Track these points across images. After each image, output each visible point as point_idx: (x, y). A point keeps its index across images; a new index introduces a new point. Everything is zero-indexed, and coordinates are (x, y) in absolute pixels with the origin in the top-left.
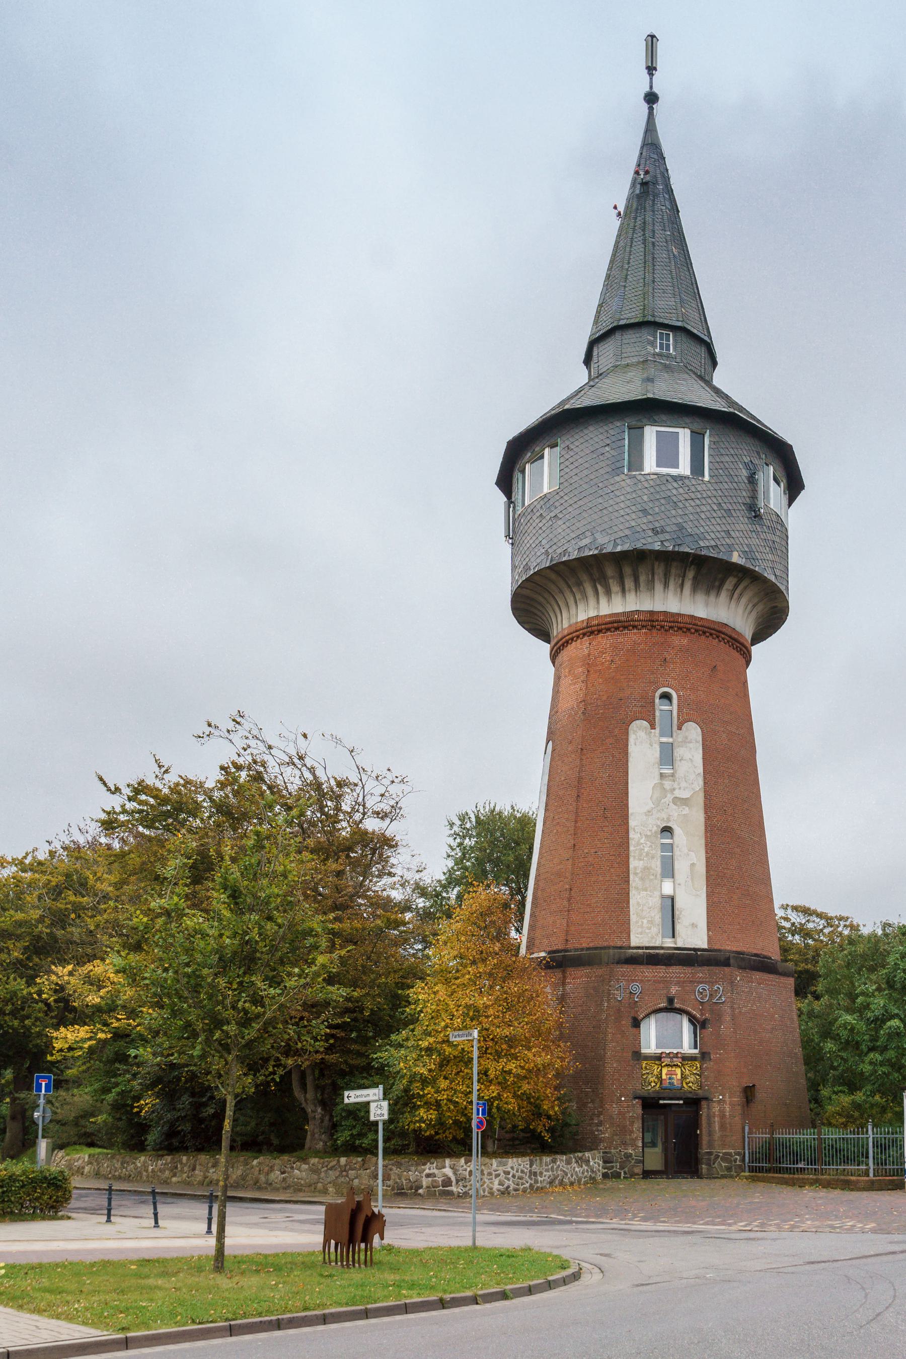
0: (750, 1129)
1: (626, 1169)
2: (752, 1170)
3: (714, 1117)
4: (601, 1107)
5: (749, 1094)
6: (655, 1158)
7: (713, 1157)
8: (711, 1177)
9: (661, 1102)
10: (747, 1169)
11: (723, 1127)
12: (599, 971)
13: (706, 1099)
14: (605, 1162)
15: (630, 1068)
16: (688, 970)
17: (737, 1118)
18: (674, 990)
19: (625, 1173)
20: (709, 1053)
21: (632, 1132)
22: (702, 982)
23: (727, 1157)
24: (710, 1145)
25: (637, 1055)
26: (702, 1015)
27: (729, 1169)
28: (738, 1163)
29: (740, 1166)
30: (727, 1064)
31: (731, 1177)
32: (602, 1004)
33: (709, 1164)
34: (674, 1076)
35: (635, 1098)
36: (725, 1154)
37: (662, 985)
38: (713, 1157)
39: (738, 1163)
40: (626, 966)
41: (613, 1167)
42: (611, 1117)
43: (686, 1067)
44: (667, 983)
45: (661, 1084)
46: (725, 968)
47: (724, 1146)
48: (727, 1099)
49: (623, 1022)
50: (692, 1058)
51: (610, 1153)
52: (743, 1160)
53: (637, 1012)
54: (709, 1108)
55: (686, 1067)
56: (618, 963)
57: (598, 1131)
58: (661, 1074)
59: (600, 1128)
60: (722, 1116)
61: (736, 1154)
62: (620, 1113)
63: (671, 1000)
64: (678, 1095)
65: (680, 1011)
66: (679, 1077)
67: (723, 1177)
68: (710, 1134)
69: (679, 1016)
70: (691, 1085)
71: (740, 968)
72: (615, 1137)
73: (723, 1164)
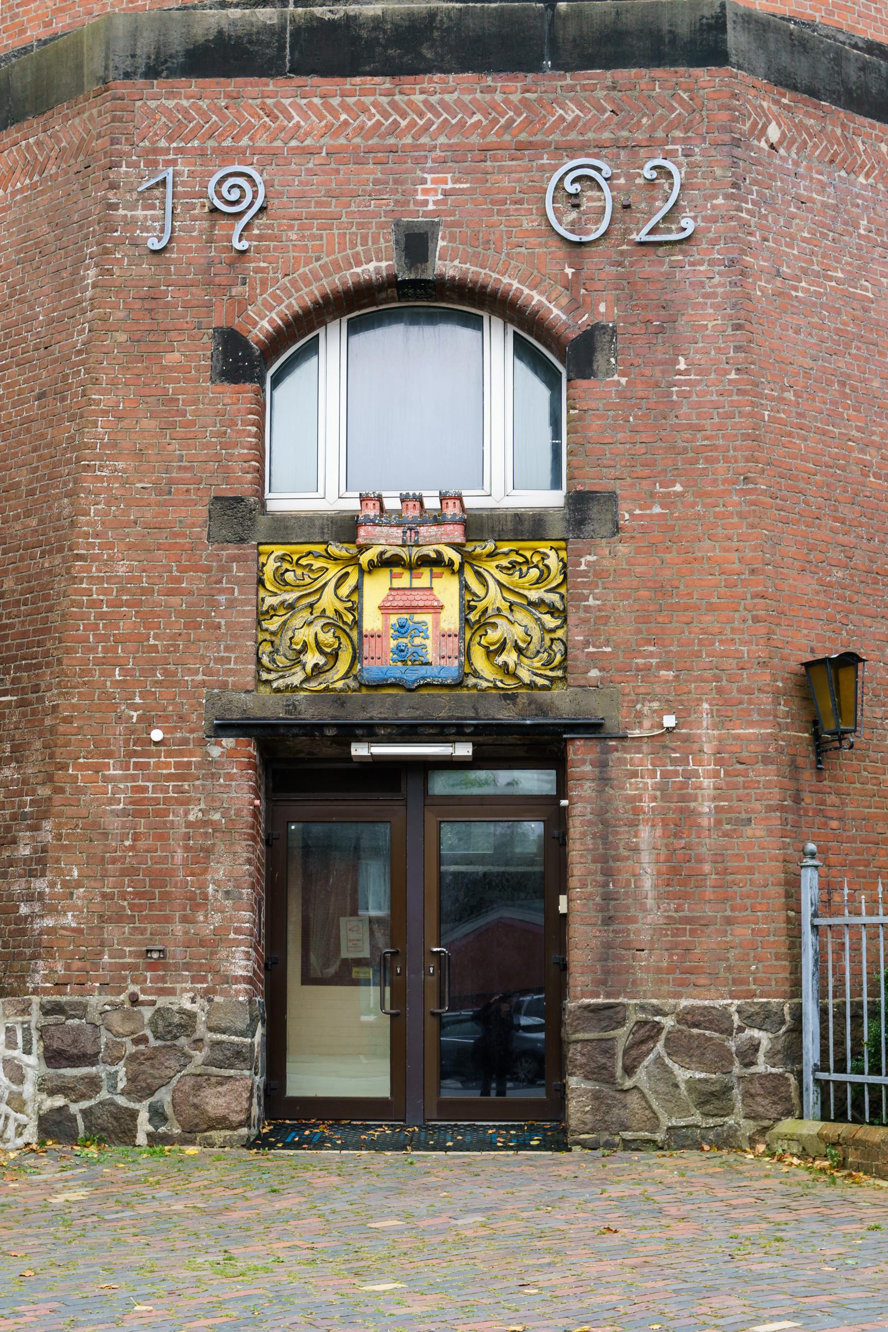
0: (828, 887)
1: (164, 1096)
2: (838, 1106)
3: (633, 824)
4: (50, 779)
5: (826, 704)
6: (346, 1048)
7: (622, 1036)
8: (615, 1138)
9: (359, 750)
10: (812, 1096)
11: (678, 874)
12: (69, 127)
13: (592, 729)
14: (53, 1057)
15: (194, 582)
16: (507, 91)
17: (756, 831)
18: (431, 193)
19: (157, 1115)
20: (612, 497)
21: (197, 902)
22: (572, 150)
23: (699, 1036)
24: (612, 968)
25: (239, 515)
26: (575, 307)
27: (713, 1099)
28: (762, 1067)
29: (774, 1087)
30: (707, 548)
31: (726, 1141)
32: (75, 281)
33: (600, 1073)
34: (417, 625)
35: (223, 729)
36: (689, 1018)
37: (372, 172)
38: (622, 1036)
39: (762, 1067)
40: (194, 85)
41: (94, 1084)
42: (95, 828)
43: (490, 567)
44: (395, 158)
45: (356, 657)
46: (702, 74)
47: (685, 975)
48: (706, 733)
49: (174, 358)
50: (528, 526)
51: (80, 1010)
52: (792, 1052)
53: (242, 305)
54: (604, 780)
55: (490, 567)
56: (152, 73)
57: (29, 898)
58: (356, 609)
59: (40, 885)
60: (679, 819)
61: (751, 1019)
62: (139, 808)
63: (416, 243)
64: (442, 715)
65: (465, 302)
66: (451, 619)
67: (681, 1140)
68: (611, 911)
69: (464, 335)
70: (514, 656)
71: (783, 80)
72: (111, 931)
73: (682, 1075)
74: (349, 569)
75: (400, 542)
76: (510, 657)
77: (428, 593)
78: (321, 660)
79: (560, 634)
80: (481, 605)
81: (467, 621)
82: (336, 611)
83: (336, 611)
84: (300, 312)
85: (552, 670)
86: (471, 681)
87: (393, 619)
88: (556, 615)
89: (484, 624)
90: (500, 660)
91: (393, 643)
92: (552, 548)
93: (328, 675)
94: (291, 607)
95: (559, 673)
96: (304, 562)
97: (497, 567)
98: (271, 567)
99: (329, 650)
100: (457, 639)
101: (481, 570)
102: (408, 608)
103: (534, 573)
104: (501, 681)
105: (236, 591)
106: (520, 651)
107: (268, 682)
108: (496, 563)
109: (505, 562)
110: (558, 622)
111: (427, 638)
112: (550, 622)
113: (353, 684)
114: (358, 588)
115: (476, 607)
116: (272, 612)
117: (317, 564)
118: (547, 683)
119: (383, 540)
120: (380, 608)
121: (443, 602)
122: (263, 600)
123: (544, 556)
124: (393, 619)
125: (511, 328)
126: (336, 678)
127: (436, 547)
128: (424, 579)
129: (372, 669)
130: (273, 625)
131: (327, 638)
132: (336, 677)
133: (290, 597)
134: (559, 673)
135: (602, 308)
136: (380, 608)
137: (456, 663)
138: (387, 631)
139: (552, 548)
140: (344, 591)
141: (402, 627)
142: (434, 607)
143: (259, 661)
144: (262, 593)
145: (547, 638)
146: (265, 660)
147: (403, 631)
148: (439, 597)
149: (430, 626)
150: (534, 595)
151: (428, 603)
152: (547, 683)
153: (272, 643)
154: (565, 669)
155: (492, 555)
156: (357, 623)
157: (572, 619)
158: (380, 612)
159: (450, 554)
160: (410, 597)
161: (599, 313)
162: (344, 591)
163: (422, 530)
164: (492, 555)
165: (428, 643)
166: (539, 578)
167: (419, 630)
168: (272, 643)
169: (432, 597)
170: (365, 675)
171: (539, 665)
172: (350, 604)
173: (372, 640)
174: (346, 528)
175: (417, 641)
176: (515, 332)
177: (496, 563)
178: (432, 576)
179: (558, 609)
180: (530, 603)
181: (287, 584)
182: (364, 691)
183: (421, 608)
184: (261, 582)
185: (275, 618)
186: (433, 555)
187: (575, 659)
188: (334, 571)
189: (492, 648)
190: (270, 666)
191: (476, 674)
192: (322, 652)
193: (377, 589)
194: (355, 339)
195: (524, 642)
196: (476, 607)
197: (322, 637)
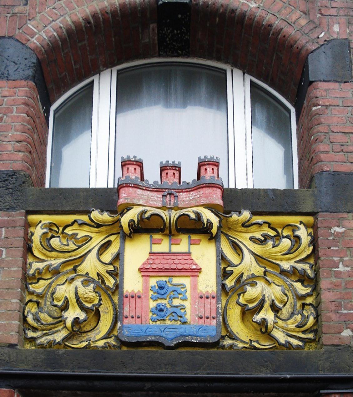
58: (116, 274)
66: (208, 282)
74: (112, 238)
75: (160, 205)
76: (267, 314)
77: (186, 258)
78: (82, 316)
79: (309, 300)
80: (237, 271)
81: (223, 286)
82: (98, 275)
83: (98, 275)
84: (73, 28)
85: (304, 332)
86: (228, 342)
87: (153, 282)
88: (306, 284)
89: (241, 284)
90: (258, 318)
91: (152, 304)
92: (301, 223)
93: (92, 335)
94: (56, 272)
95: (311, 336)
96: (69, 231)
97: (251, 239)
98: (38, 232)
99: (89, 305)
100: (214, 301)
101: (236, 241)
102: (166, 270)
103: (286, 243)
104: (257, 342)
105: (4, 253)
106: (275, 309)
107: (33, 339)
108: (249, 235)
109: (258, 235)
110: (308, 290)
111: (185, 299)
112: (301, 289)
113: (112, 341)
114: (118, 257)
115: (232, 272)
116: (38, 277)
117: (82, 233)
118: (301, 344)
119: (142, 204)
120: (141, 270)
121: (200, 265)
122: (30, 265)
123: (294, 228)
124: (153, 282)
125: (248, 78)
126: (98, 337)
127: (195, 209)
128: (183, 244)
129: (131, 329)
130: (39, 287)
131: (88, 292)
132: (98, 337)
133: (55, 263)
134: (311, 336)
135: (336, 28)
136: (141, 270)
137: (214, 322)
138: (146, 293)
139: (301, 223)
140: (107, 257)
141: (161, 288)
142: (192, 270)
143: (24, 319)
144: (30, 260)
145: (299, 304)
146: (30, 319)
147: (162, 292)
148: (197, 262)
149: (188, 287)
150: (286, 265)
151: (186, 266)
152: (301, 344)
153: (38, 303)
154: (315, 332)
155: (246, 225)
156: (118, 287)
157: (324, 284)
158: (140, 275)
159: (208, 215)
160: (169, 261)
161: (334, 32)
162: (107, 257)
163: (182, 195)
164: (246, 225)
165: (187, 304)
166: (291, 249)
167: (177, 291)
168: (38, 303)
169: (189, 262)
170: (126, 332)
171: (293, 326)
172: (111, 268)
173: (133, 300)
174: (107, 199)
175: (176, 302)
176: (252, 84)
177: (250, 235)
178: (191, 243)
179: (309, 277)
180: (283, 272)
181: (53, 250)
182: (124, 348)
183: (180, 270)
184: (29, 250)
185: (41, 282)
186: (193, 216)
187: (329, 319)
188: (98, 240)
189: (250, 306)
190: (35, 324)
191: (232, 336)
192: (83, 308)
193: (137, 252)
194: (121, 117)
195: (281, 302)
196: (232, 272)
197: (82, 290)
